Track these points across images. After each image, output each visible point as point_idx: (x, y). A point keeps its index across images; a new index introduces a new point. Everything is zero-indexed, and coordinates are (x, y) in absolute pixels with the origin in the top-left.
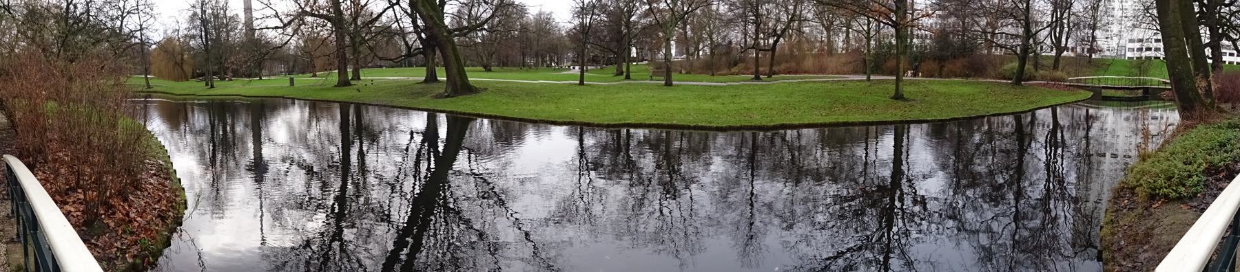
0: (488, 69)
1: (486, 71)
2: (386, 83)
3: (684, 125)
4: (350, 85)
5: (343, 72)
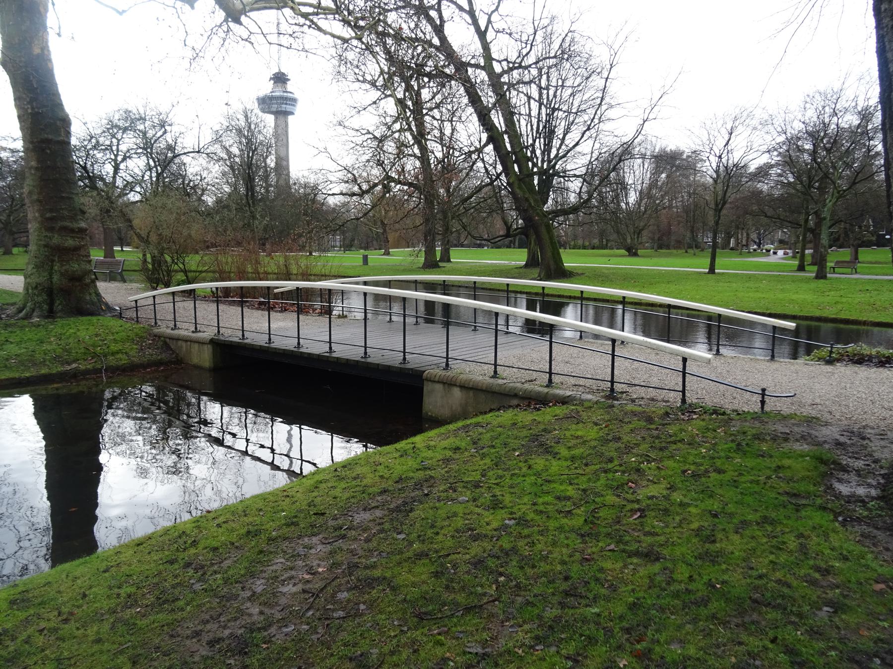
0: (632, 252)
1: (630, 255)
2: (480, 266)
3: (849, 319)
4: (439, 267)
5: (430, 251)
